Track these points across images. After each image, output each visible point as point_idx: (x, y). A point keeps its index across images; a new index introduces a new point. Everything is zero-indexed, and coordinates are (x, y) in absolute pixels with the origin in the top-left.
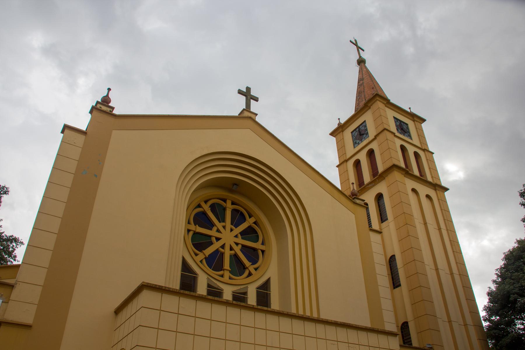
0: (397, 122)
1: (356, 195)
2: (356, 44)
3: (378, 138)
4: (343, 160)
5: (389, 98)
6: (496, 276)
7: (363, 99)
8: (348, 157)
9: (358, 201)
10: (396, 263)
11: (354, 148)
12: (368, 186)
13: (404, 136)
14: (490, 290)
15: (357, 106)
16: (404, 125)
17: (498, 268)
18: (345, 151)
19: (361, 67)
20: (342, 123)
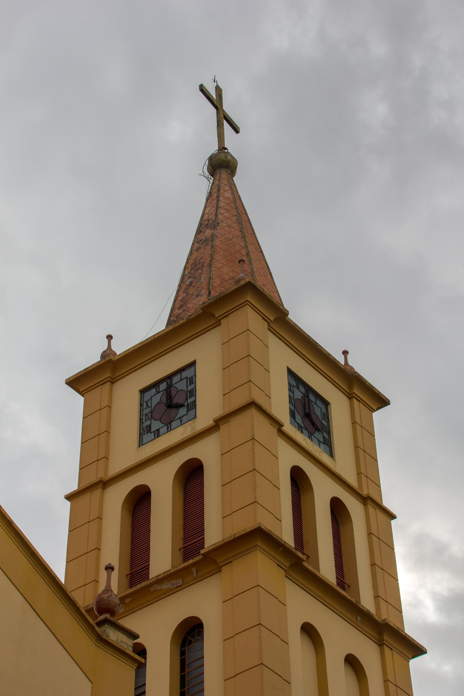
0: (295, 390)
1: (112, 612)
3: (223, 428)
4: (92, 479)
5: (287, 305)
7: (203, 292)
11: (139, 446)
12: (158, 587)
18: (109, 423)
19: (217, 182)
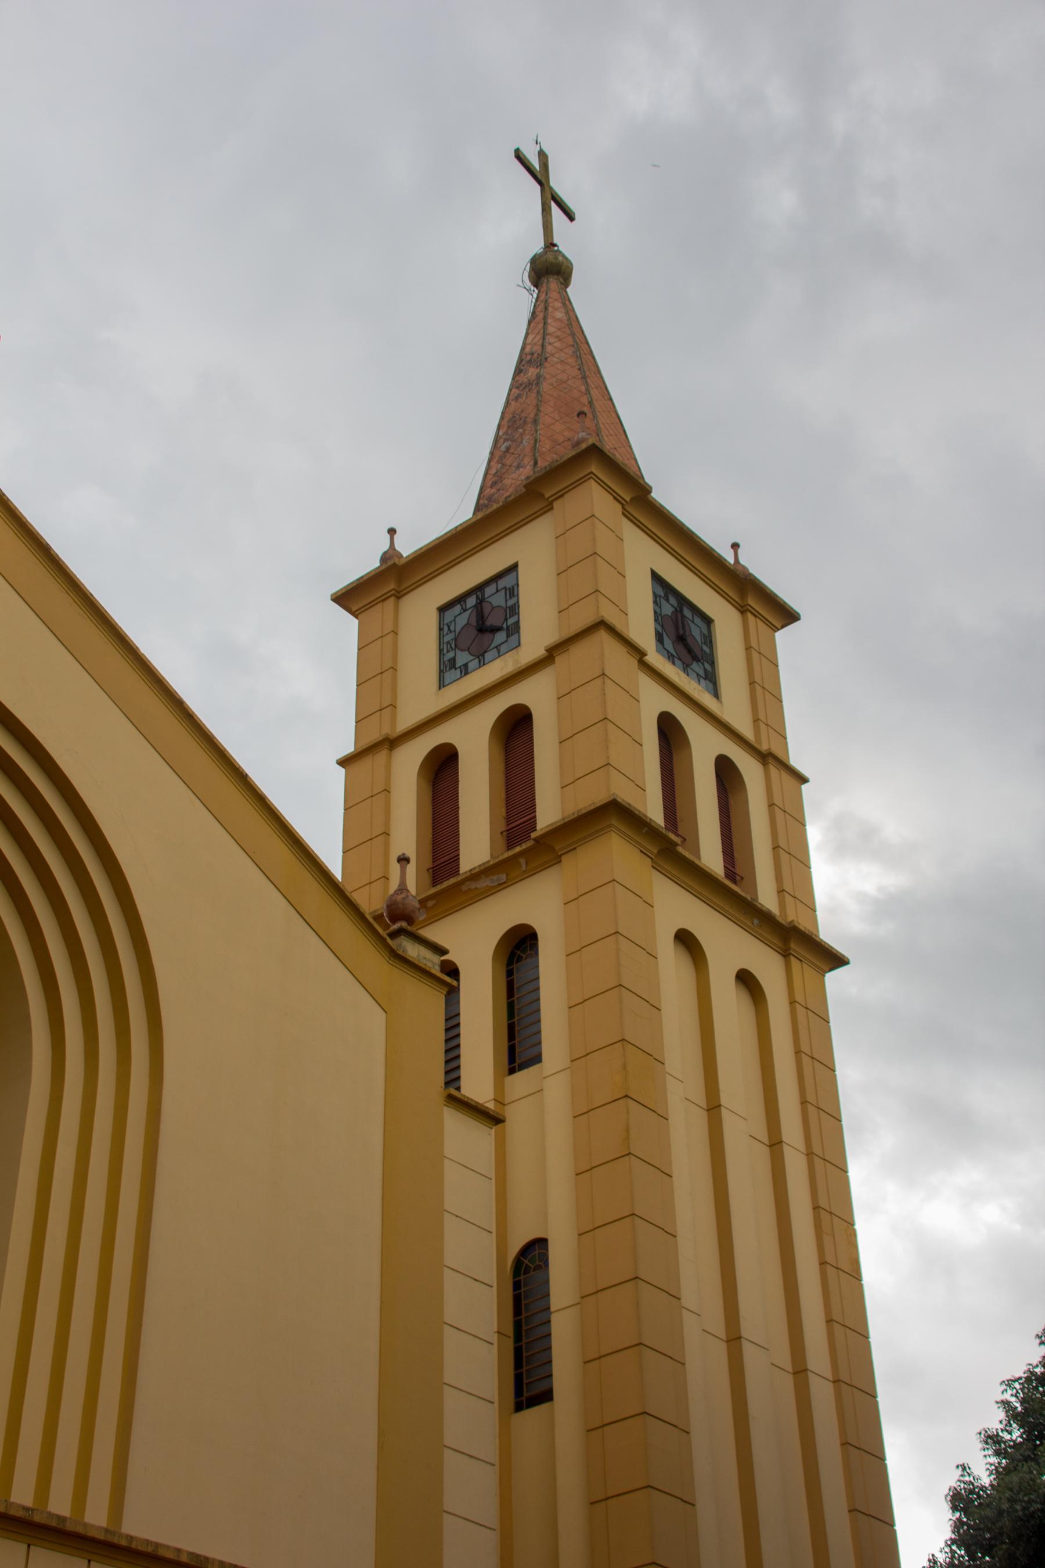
0: (663, 602)
1: (410, 920)
2: (540, 176)
3: (559, 660)
4: (374, 736)
5: (649, 478)
6: (1001, 1414)
7: (526, 461)
8: (404, 724)
9: (413, 951)
10: (547, 1282)
11: (440, 688)
12: (473, 885)
13: (683, 675)
14: (967, 1478)
15: (492, 487)
16: (693, 622)
17: (1017, 1375)
19: (543, 297)
20: (405, 555)
